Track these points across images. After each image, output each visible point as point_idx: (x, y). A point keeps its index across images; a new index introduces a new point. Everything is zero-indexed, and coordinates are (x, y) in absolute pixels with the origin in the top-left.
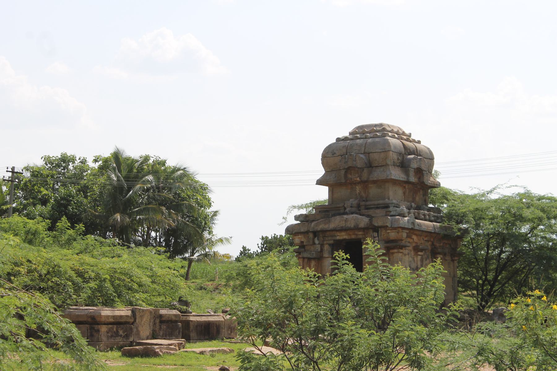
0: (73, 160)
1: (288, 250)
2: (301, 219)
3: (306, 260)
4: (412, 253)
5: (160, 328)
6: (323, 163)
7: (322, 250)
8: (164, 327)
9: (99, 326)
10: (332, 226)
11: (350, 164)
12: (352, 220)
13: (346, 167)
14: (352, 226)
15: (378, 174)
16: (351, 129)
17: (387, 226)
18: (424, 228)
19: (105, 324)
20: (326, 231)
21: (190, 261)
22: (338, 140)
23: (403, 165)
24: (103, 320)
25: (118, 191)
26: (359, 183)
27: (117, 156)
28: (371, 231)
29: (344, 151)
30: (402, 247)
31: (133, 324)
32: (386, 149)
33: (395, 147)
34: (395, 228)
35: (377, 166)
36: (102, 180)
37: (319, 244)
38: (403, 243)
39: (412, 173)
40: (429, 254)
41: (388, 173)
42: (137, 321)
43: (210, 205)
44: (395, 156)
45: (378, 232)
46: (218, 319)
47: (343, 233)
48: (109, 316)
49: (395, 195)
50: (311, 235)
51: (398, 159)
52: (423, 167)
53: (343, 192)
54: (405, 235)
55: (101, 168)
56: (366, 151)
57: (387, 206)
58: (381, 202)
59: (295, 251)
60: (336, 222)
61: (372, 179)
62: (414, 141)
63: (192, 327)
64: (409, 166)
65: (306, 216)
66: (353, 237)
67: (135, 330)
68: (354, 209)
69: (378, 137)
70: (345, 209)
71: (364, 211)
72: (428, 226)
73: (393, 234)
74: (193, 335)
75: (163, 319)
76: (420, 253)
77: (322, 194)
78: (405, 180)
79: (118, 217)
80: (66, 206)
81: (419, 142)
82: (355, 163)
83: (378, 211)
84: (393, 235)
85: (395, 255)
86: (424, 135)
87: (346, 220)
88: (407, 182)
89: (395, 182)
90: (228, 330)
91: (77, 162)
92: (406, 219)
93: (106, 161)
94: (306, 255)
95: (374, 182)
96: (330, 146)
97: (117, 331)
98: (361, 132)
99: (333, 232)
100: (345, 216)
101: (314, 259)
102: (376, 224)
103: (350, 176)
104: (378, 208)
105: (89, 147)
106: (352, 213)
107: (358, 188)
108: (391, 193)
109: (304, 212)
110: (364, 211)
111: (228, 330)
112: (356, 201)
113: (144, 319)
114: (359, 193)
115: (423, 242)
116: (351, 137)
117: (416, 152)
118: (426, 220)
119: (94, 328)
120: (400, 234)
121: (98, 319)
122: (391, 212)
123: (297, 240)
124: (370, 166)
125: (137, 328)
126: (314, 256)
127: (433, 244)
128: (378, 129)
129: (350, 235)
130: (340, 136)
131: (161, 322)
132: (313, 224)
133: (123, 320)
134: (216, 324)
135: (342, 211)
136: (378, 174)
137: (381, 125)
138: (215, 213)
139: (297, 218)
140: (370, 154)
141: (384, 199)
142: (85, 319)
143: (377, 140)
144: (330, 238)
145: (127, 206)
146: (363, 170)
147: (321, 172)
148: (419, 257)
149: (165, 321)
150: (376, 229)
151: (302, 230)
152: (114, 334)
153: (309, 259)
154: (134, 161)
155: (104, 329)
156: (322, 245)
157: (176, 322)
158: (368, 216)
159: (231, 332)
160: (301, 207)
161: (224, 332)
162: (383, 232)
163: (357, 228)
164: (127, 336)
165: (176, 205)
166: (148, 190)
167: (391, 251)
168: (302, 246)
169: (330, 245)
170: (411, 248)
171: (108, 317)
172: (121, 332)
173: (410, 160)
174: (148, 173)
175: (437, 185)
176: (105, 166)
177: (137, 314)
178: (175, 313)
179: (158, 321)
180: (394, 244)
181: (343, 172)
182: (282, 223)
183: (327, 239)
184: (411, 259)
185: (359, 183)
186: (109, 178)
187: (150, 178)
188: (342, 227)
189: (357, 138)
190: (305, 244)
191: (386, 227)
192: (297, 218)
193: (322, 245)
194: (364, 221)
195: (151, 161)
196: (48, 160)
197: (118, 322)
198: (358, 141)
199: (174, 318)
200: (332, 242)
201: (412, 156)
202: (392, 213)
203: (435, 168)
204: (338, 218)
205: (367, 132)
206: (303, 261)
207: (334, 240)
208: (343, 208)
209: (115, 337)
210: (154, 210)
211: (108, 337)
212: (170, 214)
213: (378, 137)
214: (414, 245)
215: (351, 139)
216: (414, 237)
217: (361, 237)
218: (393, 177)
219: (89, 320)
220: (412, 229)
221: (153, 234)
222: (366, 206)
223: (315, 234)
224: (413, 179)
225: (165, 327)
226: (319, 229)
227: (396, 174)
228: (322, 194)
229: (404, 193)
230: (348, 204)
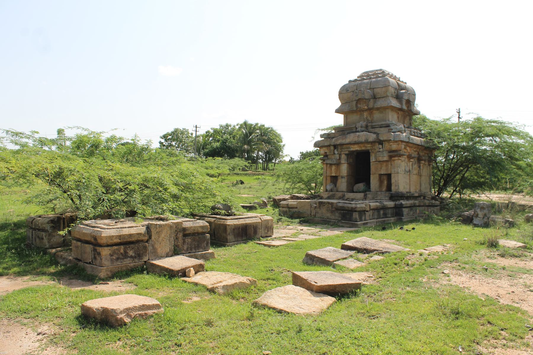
0: (230, 126)
1: (314, 159)
2: (325, 136)
3: (328, 165)
4: (407, 160)
5: (184, 242)
6: (340, 98)
7: (340, 159)
8: (189, 240)
9: (100, 248)
10: (348, 140)
11: (360, 96)
12: (363, 136)
14: (363, 140)
15: (380, 103)
16: (358, 75)
17: (390, 140)
18: (415, 142)
19: (108, 246)
20: (343, 144)
21: (275, 163)
22: (350, 81)
23: (398, 97)
24: (103, 241)
25: (246, 136)
26: (366, 110)
27: (245, 123)
28: (377, 144)
29: (355, 88)
30: (401, 155)
31: (147, 241)
32: (387, 84)
33: (393, 84)
34: (396, 142)
36: (240, 133)
38: (401, 152)
39: (404, 102)
40: (416, 160)
41: (389, 102)
42: (153, 238)
43: (282, 142)
44: (393, 90)
45: (382, 144)
46: (256, 221)
47: (356, 146)
48: (113, 236)
49: (392, 118)
50: (332, 148)
51: (395, 93)
52: (411, 100)
53: (354, 117)
54: (403, 147)
55: (239, 128)
56: (371, 87)
57: (388, 126)
58: (383, 123)
59: (321, 159)
60: (351, 138)
61: (375, 107)
62: (402, 82)
63: (229, 231)
64: (402, 98)
65: (328, 134)
66: (363, 148)
67: (150, 248)
68: (363, 129)
69: (380, 77)
70: (356, 128)
71: (371, 130)
72: (417, 140)
73: (395, 146)
74: (230, 237)
75: (187, 232)
76: (411, 160)
77: (339, 120)
78: (400, 107)
79: (246, 146)
80: (225, 143)
81: (406, 83)
83: (382, 129)
84: (394, 147)
85: (396, 161)
86: (410, 80)
87: (358, 136)
88: (401, 110)
89: (393, 108)
90: (265, 230)
91: (232, 127)
92: (404, 134)
93: (241, 125)
94: (329, 162)
95: (378, 109)
97: (126, 252)
98: (367, 75)
100: (358, 134)
101: (334, 164)
102: (382, 139)
103: (359, 106)
104: (381, 127)
105: (235, 120)
106: (363, 131)
107: (365, 114)
108: (390, 117)
109: (326, 132)
110: (371, 130)
111: (265, 230)
112: (365, 123)
113: (163, 235)
114: (366, 118)
115: (413, 152)
116: (359, 79)
117: (405, 88)
118: (415, 136)
120: (400, 146)
121: (99, 241)
122: (392, 129)
123: (322, 152)
124: (375, 97)
125: (153, 246)
126: (335, 162)
127: (418, 154)
128: (379, 72)
130: (352, 79)
131: (185, 235)
132: (334, 139)
133: (133, 239)
134: (253, 226)
135: (354, 130)
136: (380, 103)
137: (381, 70)
138: (284, 145)
139: (322, 136)
141: (386, 121)
142: (88, 238)
143: (379, 79)
145: (249, 143)
147: (338, 104)
148: (411, 163)
149: (190, 234)
150: (381, 142)
151: (326, 144)
152: (121, 256)
153: (331, 165)
154: (252, 125)
155: (105, 252)
156: (340, 155)
157: (203, 233)
158: (375, 133)
159: (268, 231)
160: (324, 130)
161: (261, 232)
162: (387, 145)
163: (367, 142)
164: (139, 256)
165: (268, 142)
166: (257, 136)
167: (393, 159)
168: (326, 156)
169: (346, 154)
170: (406, 156)
171: (111, 237)
172: (131, 253)
173: (403, 93)
174: (257, 130)
175: (418, 113)
176: (241, 127)
177: (153, 231)
178: (202, 225)
179: (180, 235)
180: (396, 153)
181: (355, 103)
182: (311, 141)
184: (406, 164)
185: (366, 110)
186: (243, 132)
187: (258, 131)
189: (364, 79)
191: (389, 141)
192: (322, 136)
193: (340, 155)
194: (372, 137)
195: (259, 125)
196: (221, 126)
197: (127, 242)
198: (365, 81)
199: (200, 230)
200: (347, 152)
201: (404, 91)
202: (393, 130)
203: (416, 103)
204: (352, 135)
205: (371, 75)
206: (327, 166)
209: (123, 259)
210: (260, 144)
211: (112, 260)
212: (266, 145)
213: (380, 77)
214: (407, 154)
215: (359, 80)
216: (408, 148)
217: (369, 148)
218: (392, 105)
219: (93, 240)
220: (408, 142)
221: (260, 153)
222: (372, 126)
223: (335, 147)
224: (405, 107)
225: (190, 240)
226: (338, 143)
227: (394, 103)
228: (339, 120)
229: (398, 117)
230: (358, 125)
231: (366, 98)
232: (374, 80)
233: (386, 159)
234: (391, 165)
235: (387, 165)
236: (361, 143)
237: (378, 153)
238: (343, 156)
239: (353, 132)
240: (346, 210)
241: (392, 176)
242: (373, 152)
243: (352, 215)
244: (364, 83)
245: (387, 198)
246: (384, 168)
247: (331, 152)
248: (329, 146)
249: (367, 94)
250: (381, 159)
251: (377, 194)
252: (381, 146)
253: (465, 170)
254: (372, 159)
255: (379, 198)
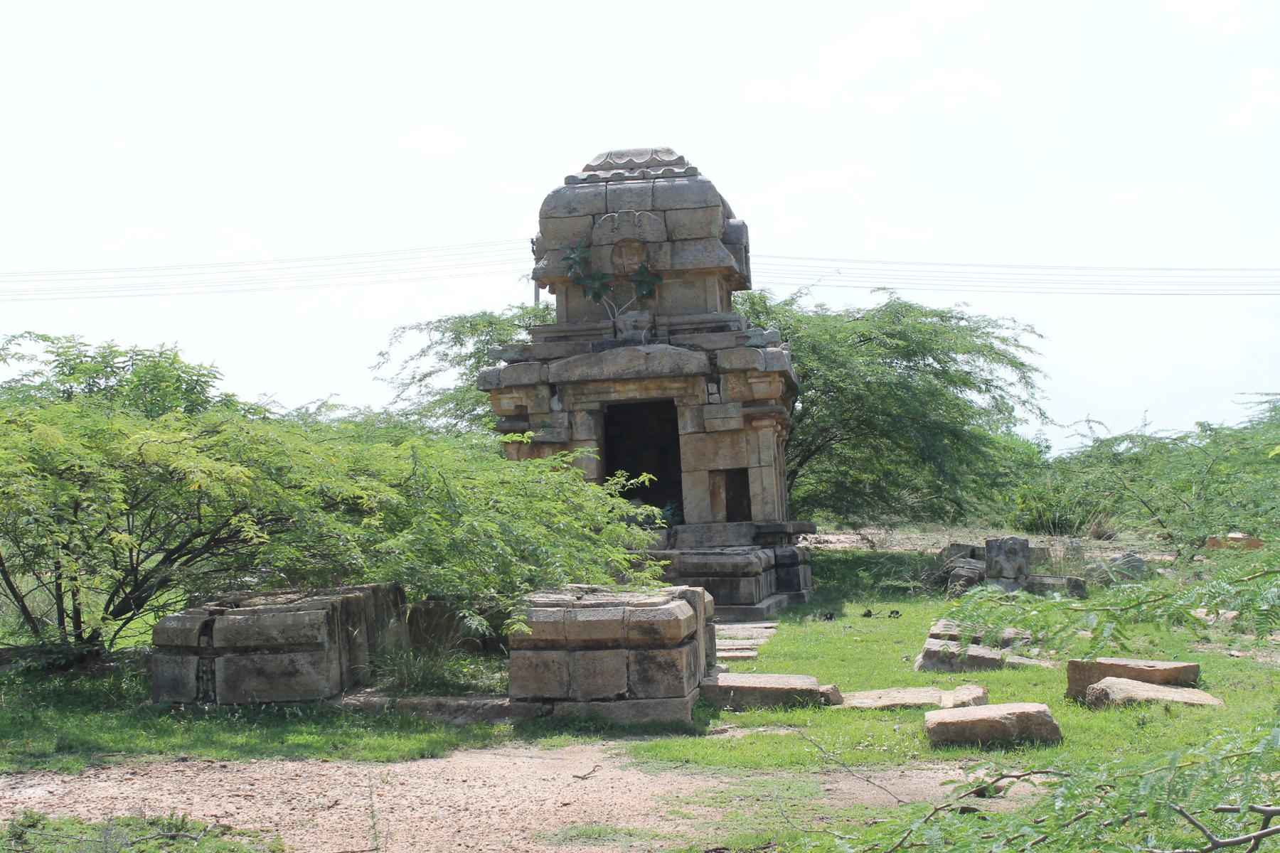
10: (609, 369)
13: (616, 240)
14: (666, 370)
16: (590, 159)
28: (702, 380)
35: (686, 240)
37: (563, 411)
45: (718, 383)
47: (632, 386)
50: (544, 392)
56: (658, 205)
66: (655, 394)
82: (638, 230)
95: (679, 274)
96: (556, 194)
99: (606, 384)
104: (697, 330)
119: (652, 659)
121: (669, 633)
129: (647, 389)
135: (608, 337)
140: (668, 213)
142: (619, 634)
144: (592, 398)
146: (661, 247)
151: (525, 381)
162: (733, 386)
163: (677, 375)
167: (754, 424)
169: (590, 412)
183: (584, 399)
188: (638, 372)
190: (529, 411)
200: (596, 406)
207: (602, 403)
208: (611, 331)
217: (674, 393)
219: (635, 635)
223: (553, 388)
231: (650, 238)
232: (661, 182)
233: (734, 424)
234: (748, 442)
235: (733, 444)
236: (658, 377)
237: (706, 408)
238: (581, 418)
239: (626, 343)
240: (716, 574)
241: (750, 471)
242: (685, 405)
243: (738, 587)
244: (630, 190)
245: (743, 541)
246: (725, 451)
247: (539, 405)
248: (534, 386)
249: (652, 230)
250: (718, 424)
251: (709, 529)
252: (713, 388)
253: (135, 558)
254: (686, 425)
255: (718, 541)
